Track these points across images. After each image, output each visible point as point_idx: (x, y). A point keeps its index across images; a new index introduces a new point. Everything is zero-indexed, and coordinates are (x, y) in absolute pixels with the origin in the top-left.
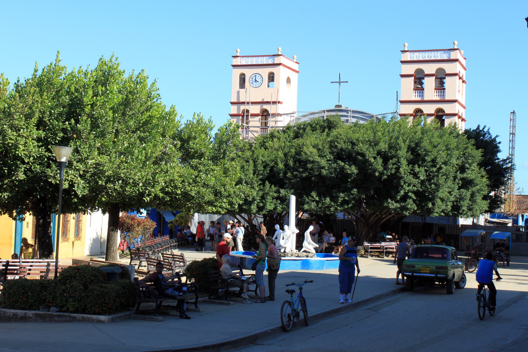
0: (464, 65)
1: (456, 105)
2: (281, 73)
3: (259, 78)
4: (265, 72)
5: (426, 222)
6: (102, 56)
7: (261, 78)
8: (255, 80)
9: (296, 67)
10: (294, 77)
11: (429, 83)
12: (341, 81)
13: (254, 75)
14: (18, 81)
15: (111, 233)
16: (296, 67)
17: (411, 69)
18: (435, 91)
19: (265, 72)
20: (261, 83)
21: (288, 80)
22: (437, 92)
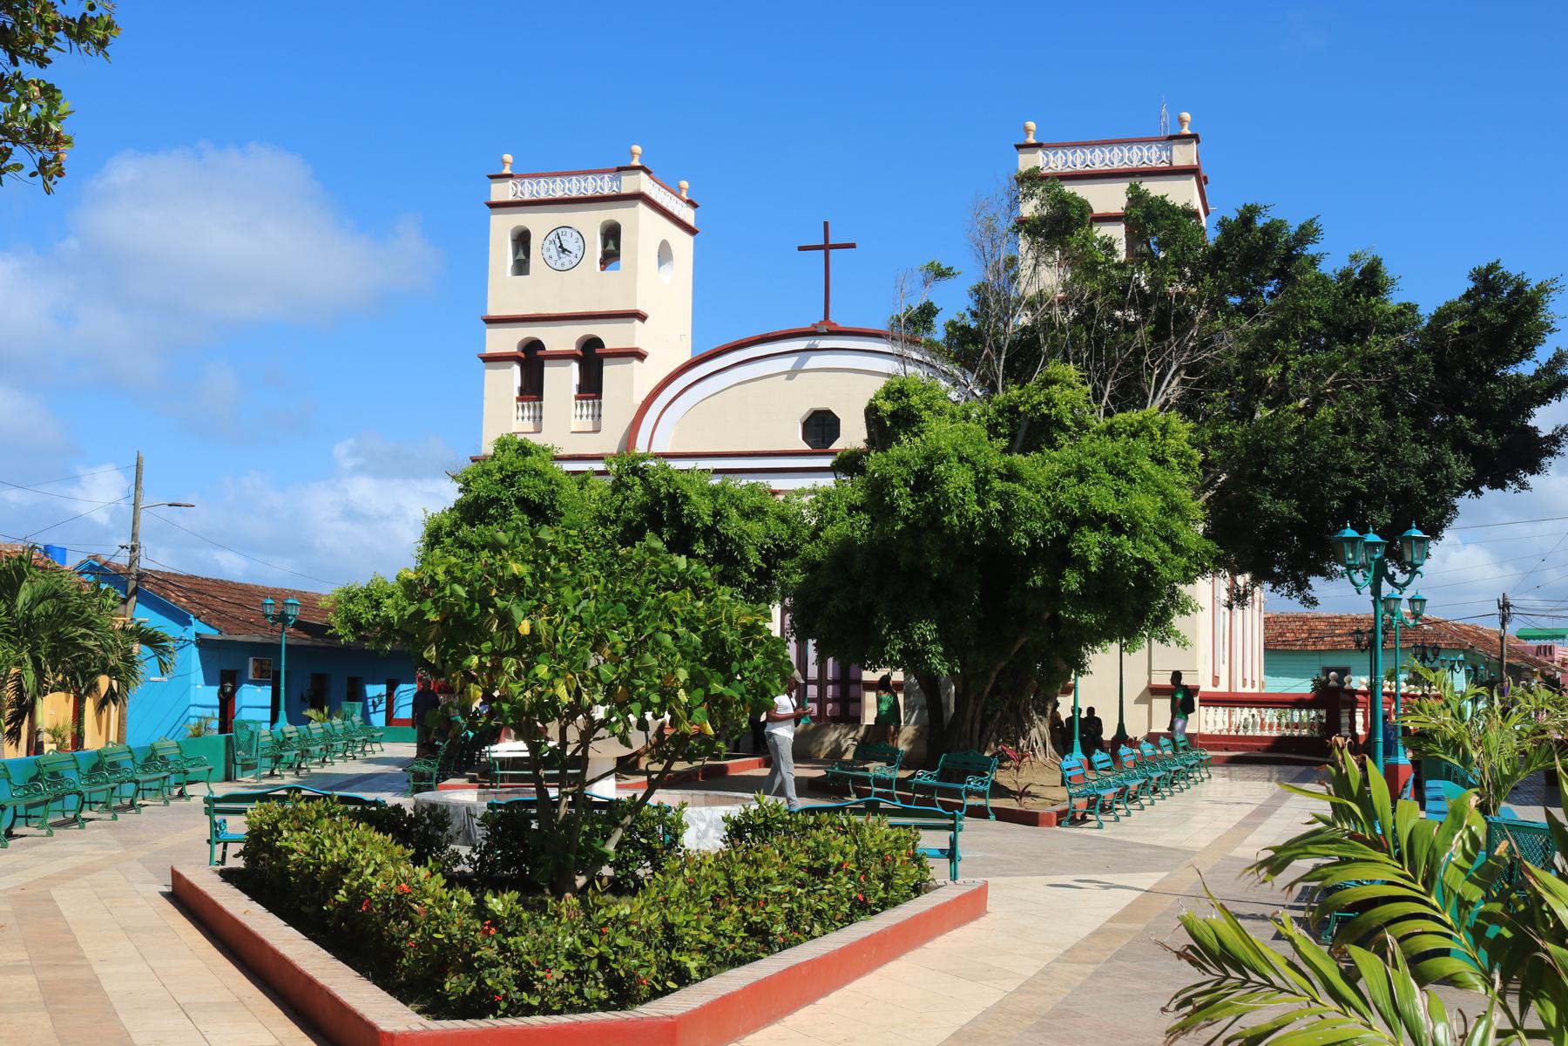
0: (1231, 1019)
1: (632, 369)
2: (642, 228)
3: (573, 240)
4: (591, 222)
5: (144, 564)
6: (92, 7)
7: (580, 240)
8: (561, 246)
9: (688, 215)
10: (683, 244)
11: (562, 380)
12: (832, 242)
13: (553, 236)
14: (1498, 262)
15: (1039, 191)
16: (688, 215)
17: (507, 340)
18: (520, 404)
19: (591, 222)
20: (579, 256)
21: (665, 254)
22: (523, 407)
